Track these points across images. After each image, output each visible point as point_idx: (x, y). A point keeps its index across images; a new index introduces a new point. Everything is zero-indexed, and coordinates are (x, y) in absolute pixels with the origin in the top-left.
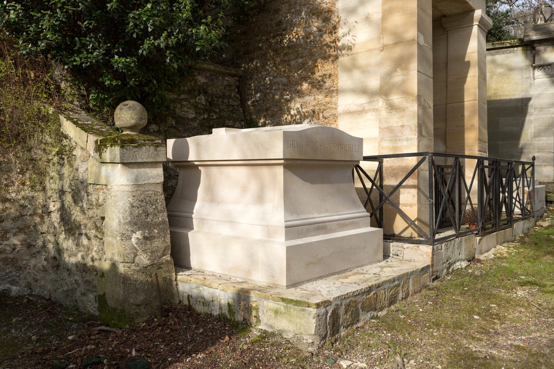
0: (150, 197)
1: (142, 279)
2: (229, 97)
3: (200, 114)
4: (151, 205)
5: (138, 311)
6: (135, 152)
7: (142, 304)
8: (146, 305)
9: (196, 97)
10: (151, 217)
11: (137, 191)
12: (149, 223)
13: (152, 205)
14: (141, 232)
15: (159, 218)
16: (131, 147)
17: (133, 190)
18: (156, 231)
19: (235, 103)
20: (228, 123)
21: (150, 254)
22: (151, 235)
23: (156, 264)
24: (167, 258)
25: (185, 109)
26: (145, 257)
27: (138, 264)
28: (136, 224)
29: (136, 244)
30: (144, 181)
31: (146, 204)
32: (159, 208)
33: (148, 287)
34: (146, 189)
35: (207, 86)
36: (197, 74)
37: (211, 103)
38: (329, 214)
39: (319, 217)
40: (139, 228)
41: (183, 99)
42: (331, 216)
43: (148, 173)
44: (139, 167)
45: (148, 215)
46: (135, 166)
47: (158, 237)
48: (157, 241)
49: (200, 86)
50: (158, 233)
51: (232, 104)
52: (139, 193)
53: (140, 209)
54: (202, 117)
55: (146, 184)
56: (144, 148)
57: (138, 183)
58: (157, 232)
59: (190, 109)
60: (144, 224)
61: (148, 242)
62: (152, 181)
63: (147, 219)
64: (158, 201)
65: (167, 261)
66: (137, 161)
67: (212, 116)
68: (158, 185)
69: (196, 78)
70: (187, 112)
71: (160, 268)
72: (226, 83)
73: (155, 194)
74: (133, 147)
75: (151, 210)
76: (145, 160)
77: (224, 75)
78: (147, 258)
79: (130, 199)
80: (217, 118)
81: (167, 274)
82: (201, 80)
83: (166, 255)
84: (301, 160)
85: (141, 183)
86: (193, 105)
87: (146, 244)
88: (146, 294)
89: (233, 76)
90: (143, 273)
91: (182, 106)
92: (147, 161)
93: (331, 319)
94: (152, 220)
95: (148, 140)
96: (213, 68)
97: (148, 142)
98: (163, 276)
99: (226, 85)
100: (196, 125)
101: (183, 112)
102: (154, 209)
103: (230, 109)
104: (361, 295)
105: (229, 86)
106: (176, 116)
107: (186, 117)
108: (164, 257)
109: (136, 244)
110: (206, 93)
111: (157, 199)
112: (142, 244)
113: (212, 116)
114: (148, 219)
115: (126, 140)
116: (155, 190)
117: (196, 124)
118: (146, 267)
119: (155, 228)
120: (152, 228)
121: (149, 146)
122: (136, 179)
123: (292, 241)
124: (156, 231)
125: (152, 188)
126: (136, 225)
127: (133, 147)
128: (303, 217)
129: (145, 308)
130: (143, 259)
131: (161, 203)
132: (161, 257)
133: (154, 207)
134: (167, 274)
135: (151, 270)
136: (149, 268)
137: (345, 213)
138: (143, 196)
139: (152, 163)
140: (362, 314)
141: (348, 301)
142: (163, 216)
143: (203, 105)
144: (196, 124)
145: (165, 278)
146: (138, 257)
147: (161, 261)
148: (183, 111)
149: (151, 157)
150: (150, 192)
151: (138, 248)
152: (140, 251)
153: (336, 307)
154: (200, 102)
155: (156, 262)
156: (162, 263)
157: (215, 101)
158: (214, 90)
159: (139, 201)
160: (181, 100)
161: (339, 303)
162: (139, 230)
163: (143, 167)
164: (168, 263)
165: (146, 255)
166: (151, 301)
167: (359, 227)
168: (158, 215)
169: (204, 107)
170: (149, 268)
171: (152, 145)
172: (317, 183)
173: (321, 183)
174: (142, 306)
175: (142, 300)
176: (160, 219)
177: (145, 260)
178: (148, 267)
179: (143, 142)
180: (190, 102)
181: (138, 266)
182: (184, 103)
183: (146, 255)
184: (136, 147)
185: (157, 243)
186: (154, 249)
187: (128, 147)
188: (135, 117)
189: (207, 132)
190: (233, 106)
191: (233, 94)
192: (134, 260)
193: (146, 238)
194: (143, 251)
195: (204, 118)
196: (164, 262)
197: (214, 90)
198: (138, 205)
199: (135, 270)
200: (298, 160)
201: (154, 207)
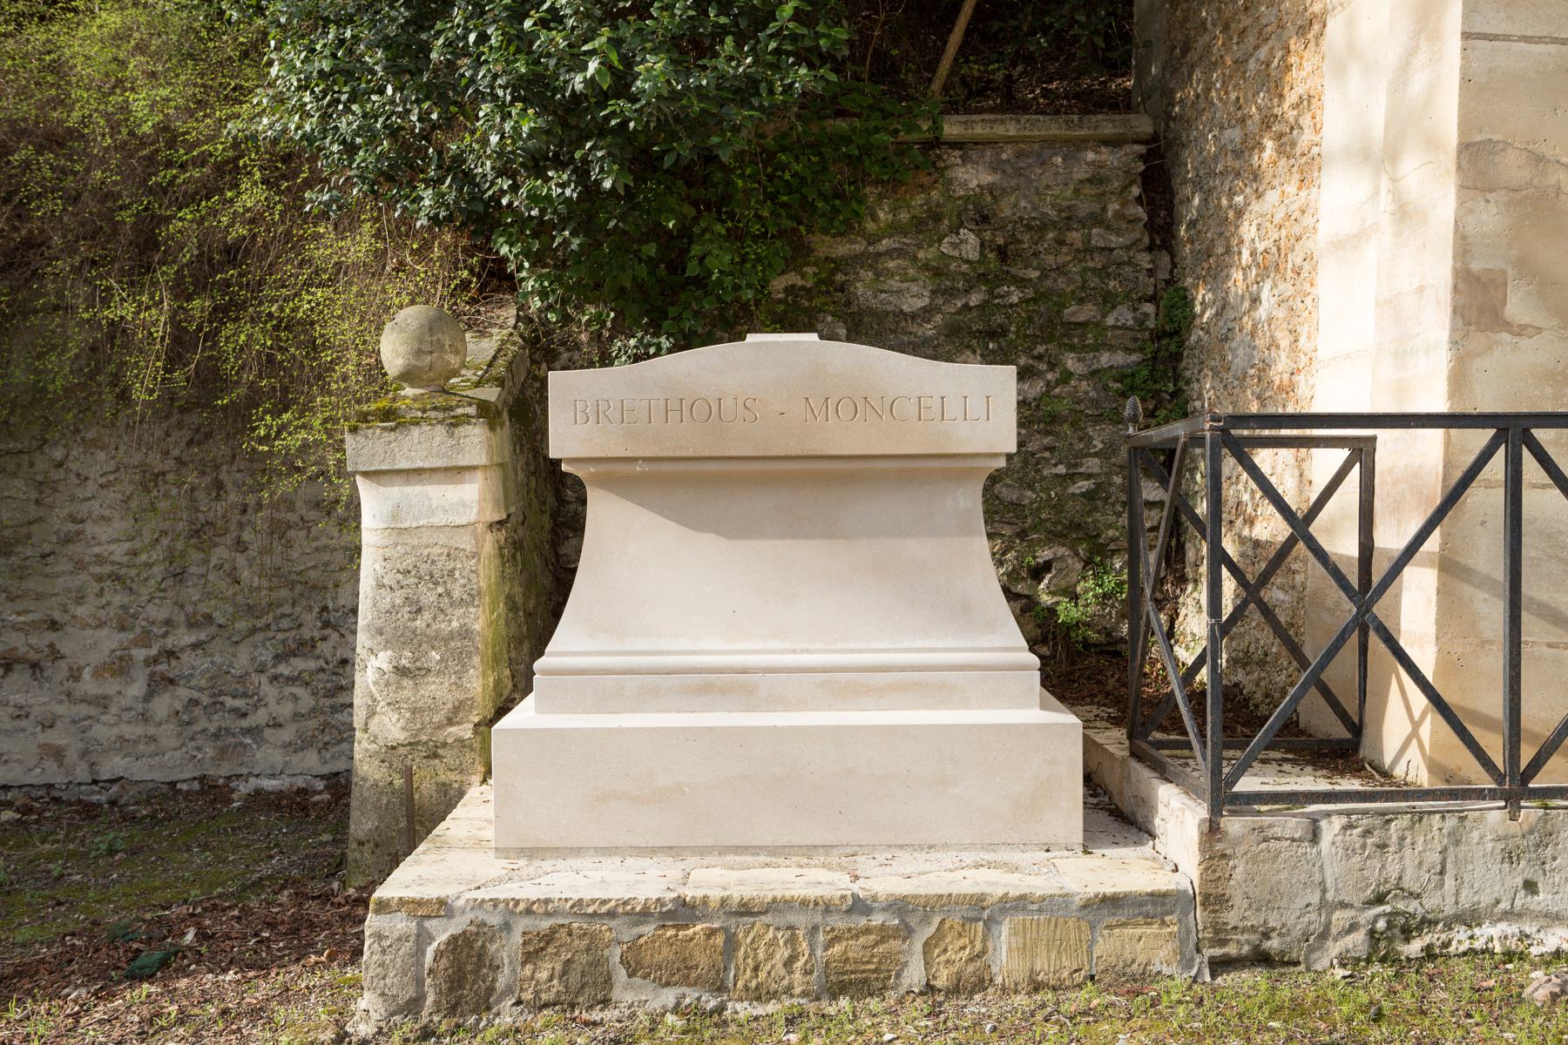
0: (433, 562)
1: (377, 777)
2: (1097, 220)
3: (950, 293)
4: (431, 586)
5: (358, 857)
6: (390, 442)
7: (368, 841)
8: (377, 845)
9: (940, 241)
10: (427, 616)
11: (396, 545)
12: (418, 631)
13: (436, 584)
14: (389, 652)
15: (450, 621)
16: (378, 431)
17: (387, 542)
18: (436, 656)
19: (1115, 240)
20: (1073, 314)
21: (408, 715)
22: (418, 664)
23: (426, 743)
24: (462, 734)
25: (894, 283)
26: (394, 720)
27: (376, 737)
28: (380, 632)
29: (376, 683)
30: (416, 519)
31: (416, 581)
32: (456, 594)
33: (389, 801)
34: (425, 541)
35: (994, 197)
36: (959, 161)
37: (1002, 253)
38: (787, 645)
39: (695, 653)
40: (387, 642)
41: (889, 253)
42: (794, 652)
43: (431, 499)
44: (407, 483)
45: (419, 610)
46: (396, 478)
47: (439, 673)
48: (434, 682)
49: (967, 199)
50: (442, 660)
51: (1102, 244)
52: (402, 551)
53: (398, 593)
54: (959, 304)
55: (422, 527)
56: (415, 431)
57: (399, 526)
58: (438, 657)
59: (914, 280)
60: (402, 635)
61: (407, 683)
62: (441, 519)
63: (414, 620)
64: (457, 573)
65: (460, 741)
66: (396, 467)
67: (1002, 297)
68: (461, 530)
69: (949, 174)
70: (899, 292)
71: (436, 756)
72: (1081, 173)
73: (448, 555)
74: (384, 429)
75: (428, 596)
76: (419, 464)
77: (1075, 146)
78: (399, 725)
79: (377, 566)
80: (1022, 301)
81: (453, 776)
82: (971, 177)
83: (459, 723)
84: (645, 459)
85: (407, 525)
86: (926, 267)
87: (399, 687)
88: (381, 818)
89: (1112, 143)
90: (383, 761)
91: (878, 275)
92: (427, 465)
93: (444, 962)
94: (428, 626)
95: (435, 408)
96: (1012, 133)
97: (433, 414)
98: (442, 778)
99: (1081, 182)
100: (930, 333)
101: (883, 295)
102: (440, 595)
103: (1091, 264)
104: (635, 918)
105: (1096, 180)
106: (854, 309)
107: (890, 308)
108: (452, 729)
109: (376, 683)
110: (984, 219)
111: (454, 569)
112: (387, 684)
113: (1002, 297)
114: (418, 622)
115: (368, 413)
116: (452, 543)
117: (929, 330)
118: (393, 748)
119: (433, 648)
120: (425, 646)
121: (431, 425)
122: (395, 516)
123: (556, 716)
124: (436, 656)
125: (443, 539)
126: (381, 634)
127: (384, 429)
128: (642, 646)
129: (373, 853)
130: (389, 726)
131: (462, 581)
132: (440, 727)
133: (440, 590)
134: (453, 776)
135: (406, 756)
136: (402, 750)
137: (907, 645)
138: (410, 560)
139: (447, 469)
140: (627, 987)
141: (546, 924)
142: (464, 616)
143: (968, 262)
144: (929, 330)
145: (444, 784)
146: (376, 719)
147: (440, 736)
148: (885, 292)
149: (438, 454)
150: (436, 550)
151: (377, 696)
152: (383, 703)
153: (473, 929)
154: (956, 254)
155: (424, 738)
156: (445, 745)
157: (1020, 242)
158: (1023, 204)
159: (399, 571)
160: (879, 255)
161: (495, 920)
162: (386, 648)
163: (421, 482)
164: (463, 747)
165: (397, 716)
166: (392, 838)
167: (965, 704)
168: (449, 611)
169: (974, 269)
170: (402, 750)
171: (441, 422)
172: (761, 535)
173: (782, 536)
174: (367, 846)
175: (370, 830)
176: (455, 624)
177: (392, 728)
178: (401, 749)
179: (419, 414)
180: (915, 258)
181: (374, 742)
182: (891, 265)
183: (397, 716)
184: (393, 429)
185: (433, 687)
186: (420, 704)
187: (370, 431)
188: (402, 350)
189: (974, 352)
190: (1111, 250)
191: (1113, 207)
192: (366, 724)
193: (401, 671)
194: (389, 704)
195: (966, 306)
196: (450, 741)
197: (1023, 204)
198: (393, 583)
199: (367, 750)
200: (634, 460)
201: (440, 590)
